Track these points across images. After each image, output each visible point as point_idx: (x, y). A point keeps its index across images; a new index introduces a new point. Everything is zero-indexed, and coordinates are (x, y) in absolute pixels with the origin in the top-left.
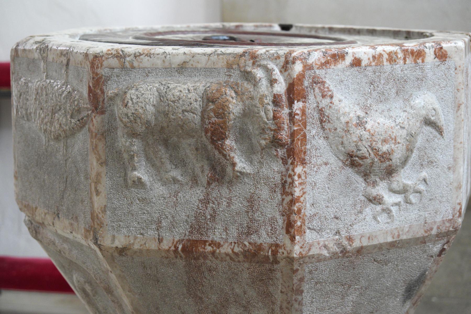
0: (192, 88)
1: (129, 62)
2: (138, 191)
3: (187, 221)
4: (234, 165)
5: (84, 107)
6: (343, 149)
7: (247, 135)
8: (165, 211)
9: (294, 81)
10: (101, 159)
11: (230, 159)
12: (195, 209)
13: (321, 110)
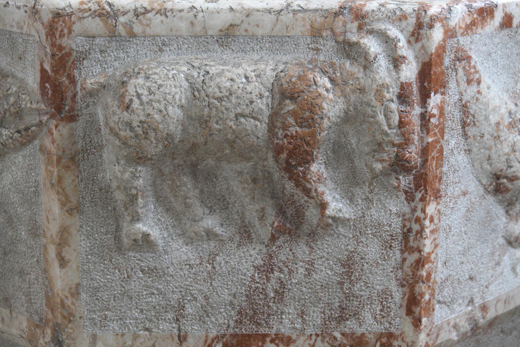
0: (253, 74)
1: (125, 25)
2: (141, 256)
3: (231, 303)
4: (323, 206)
5: (31, 108)
6: (488, 167)
7: (345, 153)
8: (191, 288)
9: (431, 59)
10: (70, 202)
11: (317, 196)
12: (247, 283)
13: (465, 106)
